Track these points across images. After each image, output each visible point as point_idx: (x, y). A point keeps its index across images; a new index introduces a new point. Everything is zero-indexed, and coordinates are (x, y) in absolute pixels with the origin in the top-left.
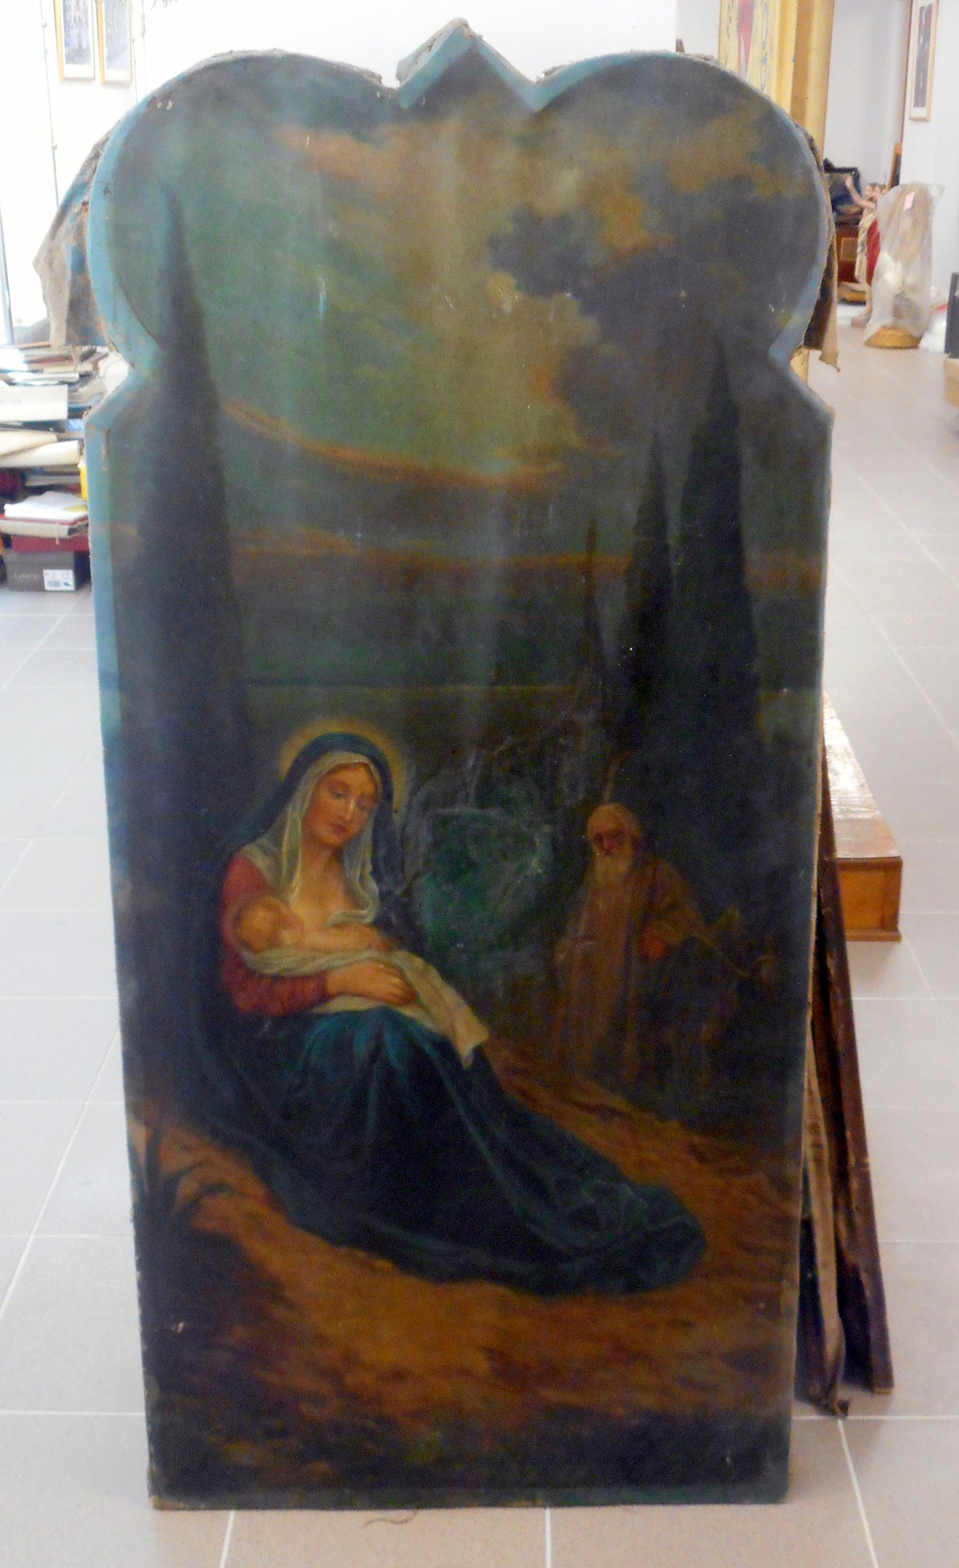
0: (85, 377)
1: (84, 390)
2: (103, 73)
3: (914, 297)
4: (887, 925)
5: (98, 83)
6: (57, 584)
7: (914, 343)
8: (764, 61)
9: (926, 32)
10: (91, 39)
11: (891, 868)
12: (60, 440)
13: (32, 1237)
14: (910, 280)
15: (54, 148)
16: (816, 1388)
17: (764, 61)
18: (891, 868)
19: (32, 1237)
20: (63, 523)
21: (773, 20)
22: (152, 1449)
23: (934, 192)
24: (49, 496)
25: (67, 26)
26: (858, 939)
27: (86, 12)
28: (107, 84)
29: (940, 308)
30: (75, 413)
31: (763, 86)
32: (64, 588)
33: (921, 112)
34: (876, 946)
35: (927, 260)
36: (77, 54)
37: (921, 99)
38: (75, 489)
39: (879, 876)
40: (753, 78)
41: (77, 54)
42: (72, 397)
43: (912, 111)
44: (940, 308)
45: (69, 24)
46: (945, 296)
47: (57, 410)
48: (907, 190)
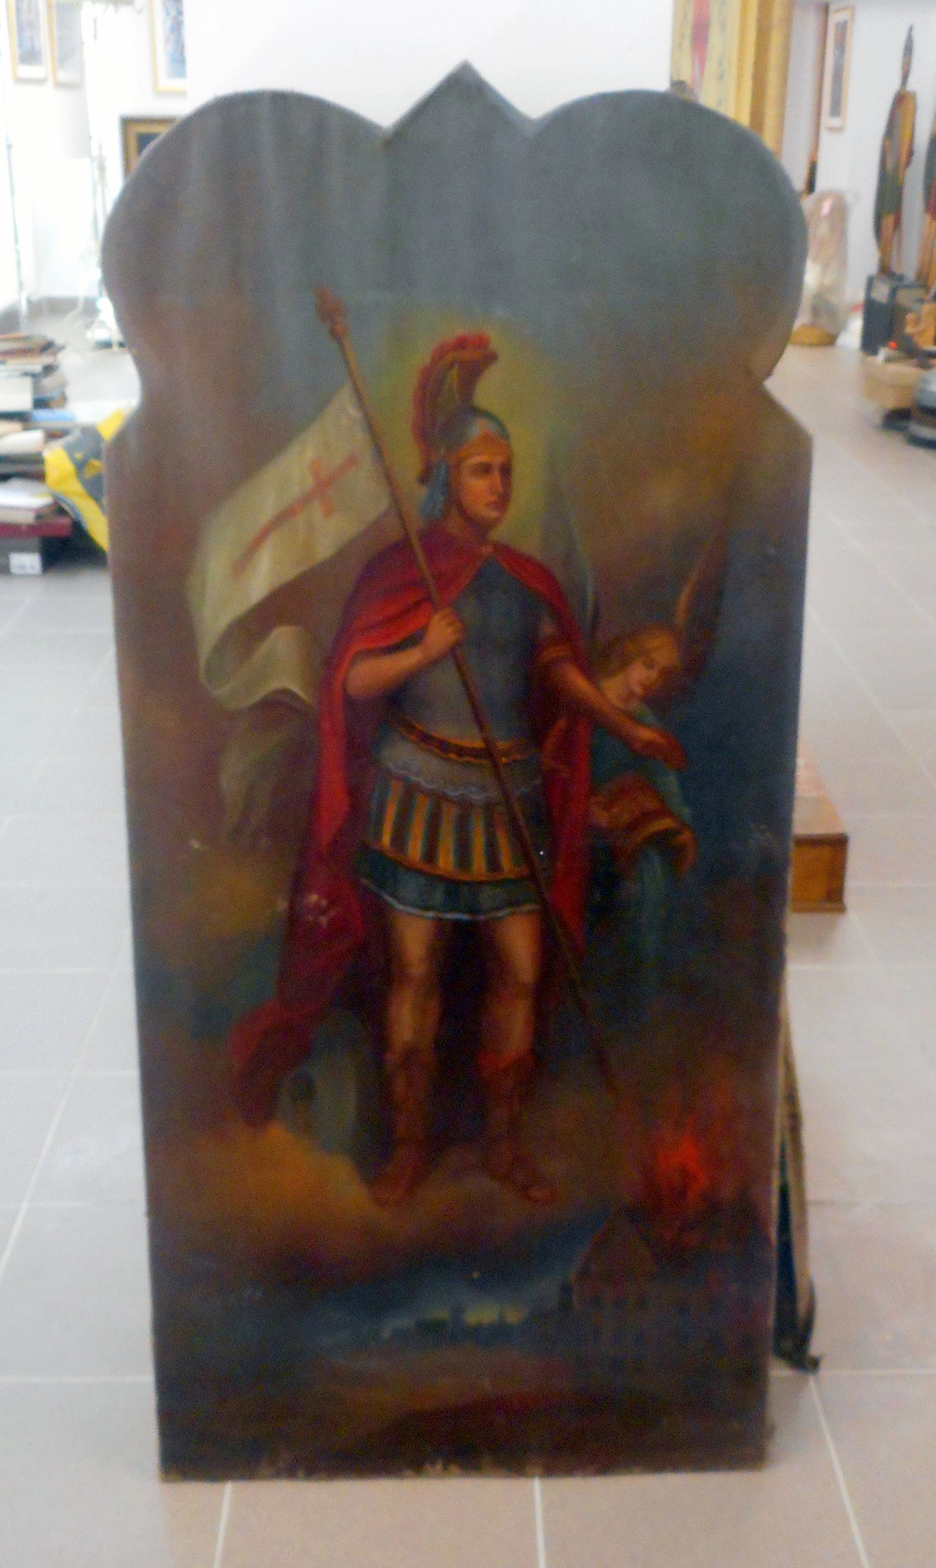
0: (49, 369)
1: (47, 382)
2: (55, 75)
3: (834, 299)
4: (832, 897)
5: (50, 84)
6: (23, 567)
7: (829, 340)
8: (721, 77)
9: (841, 45)
10: (44, 41)
11: (837, 845)
12: (26, 429)
13: (25, 1206)
14: (828, 281)
15: (9, 147)
16: (788, 1344)
17: (721, 77)
18: (837, 845)
19: (25, 1206)
20: (28, 510)
21: (730, 41)
22: (408, 1472)
23: (849, 199)
24: (15, 483)
25: (20, 28)
26: (799, 910)
27: (37, 14)
28: (59, 85)
29: (855, 308)
30: (40, 403)
31: (720, 103)
32: (30, 571)
33: (835, 122)
34: (827, 916)
35: (843, 264)
36: (29, 56)
37: (837, 108)
38: (39, 477)
39: (826, 852)
40: (708, 98)
41: (29, 56)
42: (36, 387)
43: (827, 120)
44: (855, 308)
45: (23, 26)
46: (860, 297)
47: (22, 400)
48: (824, 196)
